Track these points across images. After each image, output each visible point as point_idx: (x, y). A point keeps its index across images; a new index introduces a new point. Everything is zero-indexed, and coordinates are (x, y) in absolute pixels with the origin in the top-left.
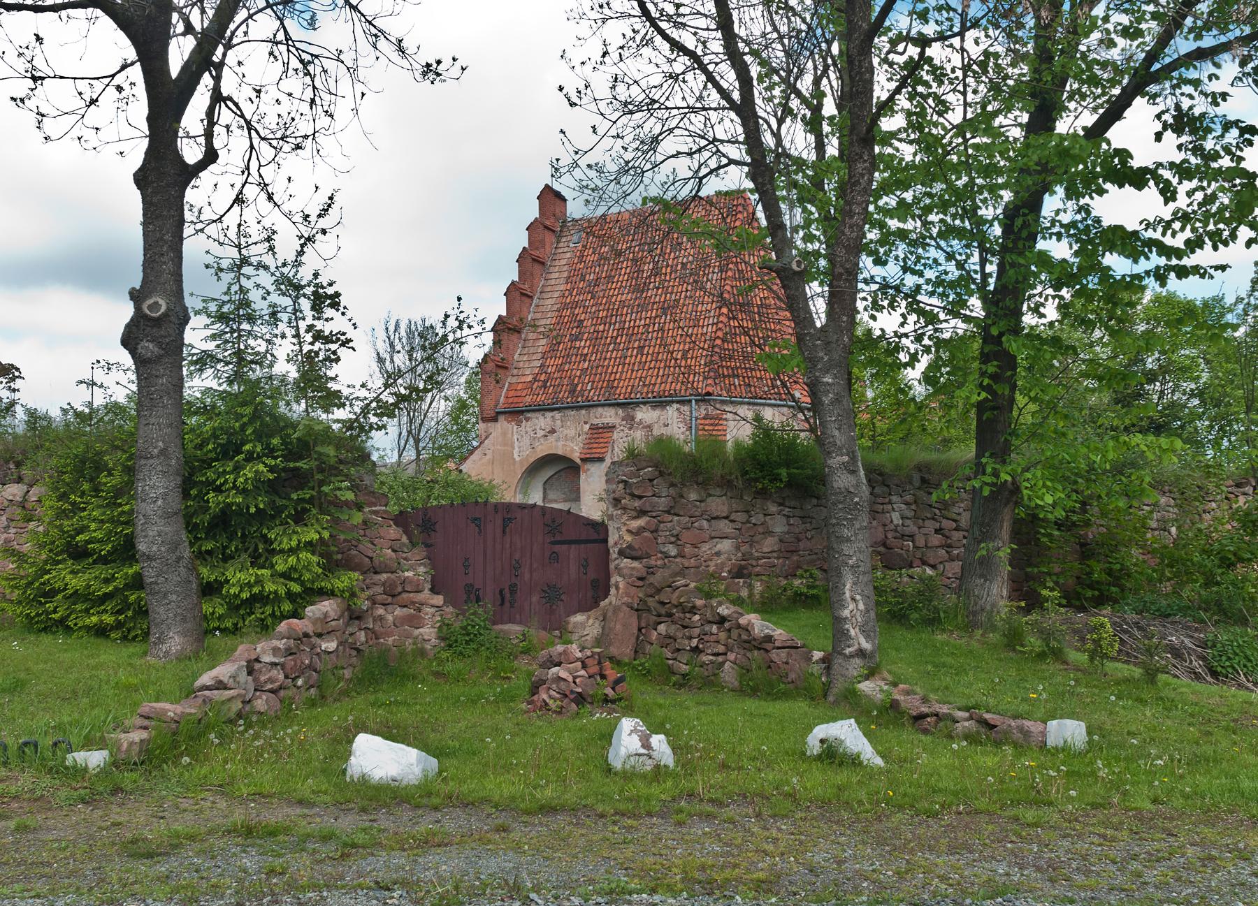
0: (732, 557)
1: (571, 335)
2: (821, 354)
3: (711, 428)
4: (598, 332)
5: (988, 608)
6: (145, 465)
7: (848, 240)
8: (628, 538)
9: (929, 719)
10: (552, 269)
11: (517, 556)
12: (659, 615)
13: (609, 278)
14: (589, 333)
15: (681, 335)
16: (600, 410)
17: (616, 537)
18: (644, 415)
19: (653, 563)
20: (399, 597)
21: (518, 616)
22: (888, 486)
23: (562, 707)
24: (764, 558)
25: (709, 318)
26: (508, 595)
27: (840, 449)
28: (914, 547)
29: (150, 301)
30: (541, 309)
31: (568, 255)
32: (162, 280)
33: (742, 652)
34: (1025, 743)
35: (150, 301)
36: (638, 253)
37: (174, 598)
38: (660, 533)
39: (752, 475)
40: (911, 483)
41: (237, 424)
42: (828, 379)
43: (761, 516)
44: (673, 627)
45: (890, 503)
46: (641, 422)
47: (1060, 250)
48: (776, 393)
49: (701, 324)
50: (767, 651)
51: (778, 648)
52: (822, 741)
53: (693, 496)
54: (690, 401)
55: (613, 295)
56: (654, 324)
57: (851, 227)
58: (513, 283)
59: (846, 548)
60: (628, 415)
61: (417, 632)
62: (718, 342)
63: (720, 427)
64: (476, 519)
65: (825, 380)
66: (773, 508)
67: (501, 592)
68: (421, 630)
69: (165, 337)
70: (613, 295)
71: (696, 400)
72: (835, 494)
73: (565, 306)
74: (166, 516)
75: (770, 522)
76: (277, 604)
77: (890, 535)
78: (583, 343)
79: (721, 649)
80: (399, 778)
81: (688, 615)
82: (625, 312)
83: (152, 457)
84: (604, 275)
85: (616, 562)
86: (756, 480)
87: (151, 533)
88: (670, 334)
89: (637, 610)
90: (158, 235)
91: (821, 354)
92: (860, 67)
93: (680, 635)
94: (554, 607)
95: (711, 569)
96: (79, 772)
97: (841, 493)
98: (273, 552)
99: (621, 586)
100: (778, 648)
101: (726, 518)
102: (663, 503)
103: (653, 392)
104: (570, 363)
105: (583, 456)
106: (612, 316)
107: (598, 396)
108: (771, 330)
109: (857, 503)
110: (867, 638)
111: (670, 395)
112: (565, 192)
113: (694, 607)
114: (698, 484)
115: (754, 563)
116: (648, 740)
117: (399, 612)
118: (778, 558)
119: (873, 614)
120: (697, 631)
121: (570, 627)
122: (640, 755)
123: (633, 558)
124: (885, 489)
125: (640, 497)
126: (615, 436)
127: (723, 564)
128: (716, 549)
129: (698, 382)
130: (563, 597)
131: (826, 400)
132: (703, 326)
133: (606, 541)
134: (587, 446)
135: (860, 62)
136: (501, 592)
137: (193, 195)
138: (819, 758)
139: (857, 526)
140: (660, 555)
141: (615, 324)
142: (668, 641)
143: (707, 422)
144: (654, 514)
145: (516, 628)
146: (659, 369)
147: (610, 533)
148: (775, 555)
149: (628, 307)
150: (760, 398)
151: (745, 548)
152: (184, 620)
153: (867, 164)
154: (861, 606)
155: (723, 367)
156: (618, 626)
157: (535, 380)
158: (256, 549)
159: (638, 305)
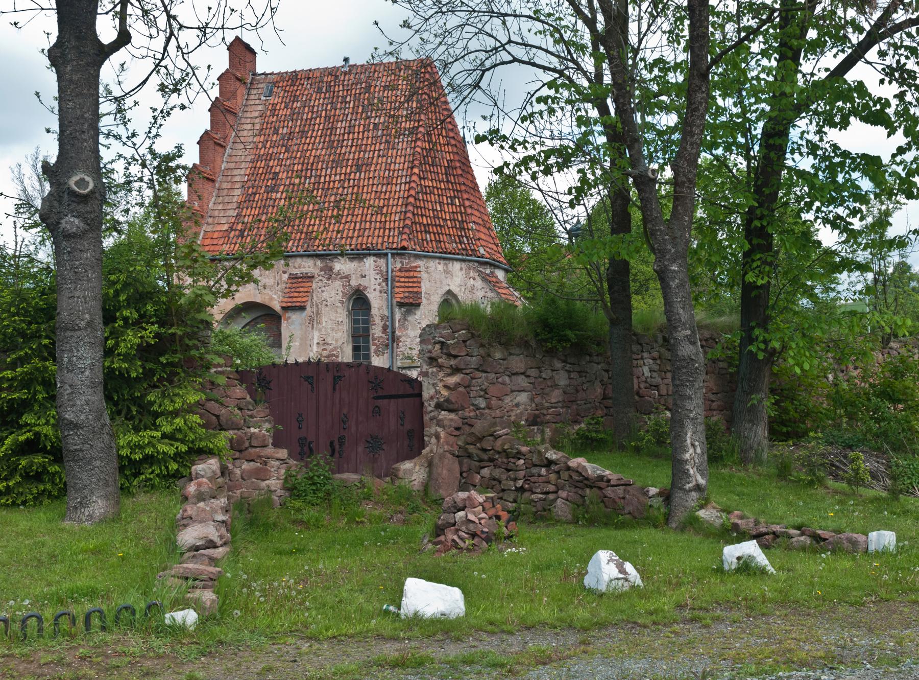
0: (528, 407)
1: (266, 186)
2: (669, 247)
3: (406, 280)
4: (294, 185)
5: (755, 446)
6: (72, 337)
7: (690, 155)
8: (445, 393)
9: (767, 537)
10: (243, 121)
11: (345, 411)
12: (481, 461)
13: (303, 133)
14: (285, 185)
15: (376, 192)
16: (299, 260)
17: (432, 392)
18: (341, 266)
19: (467, 414)
20: (246, 452)
21: (345, 466)
22: (641, 345)
23: (474, 545)
24: (552, 407)
25: (402, 176)
26: (337, 447)
27: (684, 324)
28: (659, 395)
29: (76, 178)
30: (234, 159)
31: (260, 108)
32: (83, 157)
33: (573, 490)
34: (854, 548)
35: (76, 178)
36: (331, 111)
37: (98, 463)
38: (472, 388)
39: (543, 336)
40: (656, 342)
41: (112, 291)
42: (674, 268)
43: (549, 371)
44: (498, 470)
45: (642, 358)
46: (339, 273)
47: (806, 164)
48: (463, 249)
49: (394, 182)
50: (600, 488)
51: (613, 486)
52: (739, 558)
53: (498, 355)
54: (386, 254)
55: (307, 150)
56: (349, 180)
57: (692, 144)
58: (206, 132)
59: (689, 405)
60: (327, 266)
61: (263, 484)
62: (411, 200)
63: (415, 280)
64: (309, 378)
65: (673, 268)
66: (558, 365)
67: (332, 443)
68: (267, 482)
69: (91, 213)
70: (307, 150)
71: (393, 254)
72: (680, 361)
73: (259, 158)
74: (93, 385)
75: (557, 377)
76: (163, 464)
77: (642, 386)
78: (279, 195)
79: (551, 488)
80: (447, 612)
81: (512, 460)
82: (319, 167)
83: (80, 329)
84: (297, 130)
85: (432, 414)
86: (546, 341)
87: (78, 403)
88: (365, 190)
89: (458, 457)
90: (79, 113)
91: (669, 247)
92: (700, 15)
93: (504, 477)
94: (377, 456)
95: (513, 418)
96: (178, 630)
97: (685, 360)
98: (156, 415)
99: (442, 435)
100: (613, 486)
101: (522, 374)
102: (474, 361)
103: (350, 245)
104: (267, 214)
105: (284, 305)
106: (307, 170)
107: (297, 246)
108: (457, 191)
109: (697, 368)
110: (702, 475)
111: (368, 249)
112: (255, 45)
113: (519, 452)
114: (501, 344)
115: (545, 412)
116: (622, 567)
117: (246, 466)
118: (562, 407)
119: (706, 457)
120: (522, 473)
121: (401, 474)
122: (618, 579)
123: (450, 411)
124: (639, 347)
125: (455, 357)
126: (314, 285)
127: (521, 413)
128: (516, 401)
129: (394, 236)
130: (384, 447)
131: (673, 284)
132: (396, 185)
133: (420, 395)
134: (287, 295)
135: (700, 11)
136: (332, 443)
137: (108, 72)
138: (738, 570)
139: (697, 386)
140: (472, 407)
141: (310, 178)
142: (494, 483)
143: (403, 274)
144: (468, 371)
145: (353, 477)
146: (355, 223)
147: (424, 388)
148: (560, 404)
149: (323, 161)
150: (450, 253)
151: (538, 400)
152: (107, 485)
153: (704, 95)
154: (699, 450)
155: (416, 224)
156: (444, 472)
157: (231, 229)
158: (129, 410)
159: (333, 161)
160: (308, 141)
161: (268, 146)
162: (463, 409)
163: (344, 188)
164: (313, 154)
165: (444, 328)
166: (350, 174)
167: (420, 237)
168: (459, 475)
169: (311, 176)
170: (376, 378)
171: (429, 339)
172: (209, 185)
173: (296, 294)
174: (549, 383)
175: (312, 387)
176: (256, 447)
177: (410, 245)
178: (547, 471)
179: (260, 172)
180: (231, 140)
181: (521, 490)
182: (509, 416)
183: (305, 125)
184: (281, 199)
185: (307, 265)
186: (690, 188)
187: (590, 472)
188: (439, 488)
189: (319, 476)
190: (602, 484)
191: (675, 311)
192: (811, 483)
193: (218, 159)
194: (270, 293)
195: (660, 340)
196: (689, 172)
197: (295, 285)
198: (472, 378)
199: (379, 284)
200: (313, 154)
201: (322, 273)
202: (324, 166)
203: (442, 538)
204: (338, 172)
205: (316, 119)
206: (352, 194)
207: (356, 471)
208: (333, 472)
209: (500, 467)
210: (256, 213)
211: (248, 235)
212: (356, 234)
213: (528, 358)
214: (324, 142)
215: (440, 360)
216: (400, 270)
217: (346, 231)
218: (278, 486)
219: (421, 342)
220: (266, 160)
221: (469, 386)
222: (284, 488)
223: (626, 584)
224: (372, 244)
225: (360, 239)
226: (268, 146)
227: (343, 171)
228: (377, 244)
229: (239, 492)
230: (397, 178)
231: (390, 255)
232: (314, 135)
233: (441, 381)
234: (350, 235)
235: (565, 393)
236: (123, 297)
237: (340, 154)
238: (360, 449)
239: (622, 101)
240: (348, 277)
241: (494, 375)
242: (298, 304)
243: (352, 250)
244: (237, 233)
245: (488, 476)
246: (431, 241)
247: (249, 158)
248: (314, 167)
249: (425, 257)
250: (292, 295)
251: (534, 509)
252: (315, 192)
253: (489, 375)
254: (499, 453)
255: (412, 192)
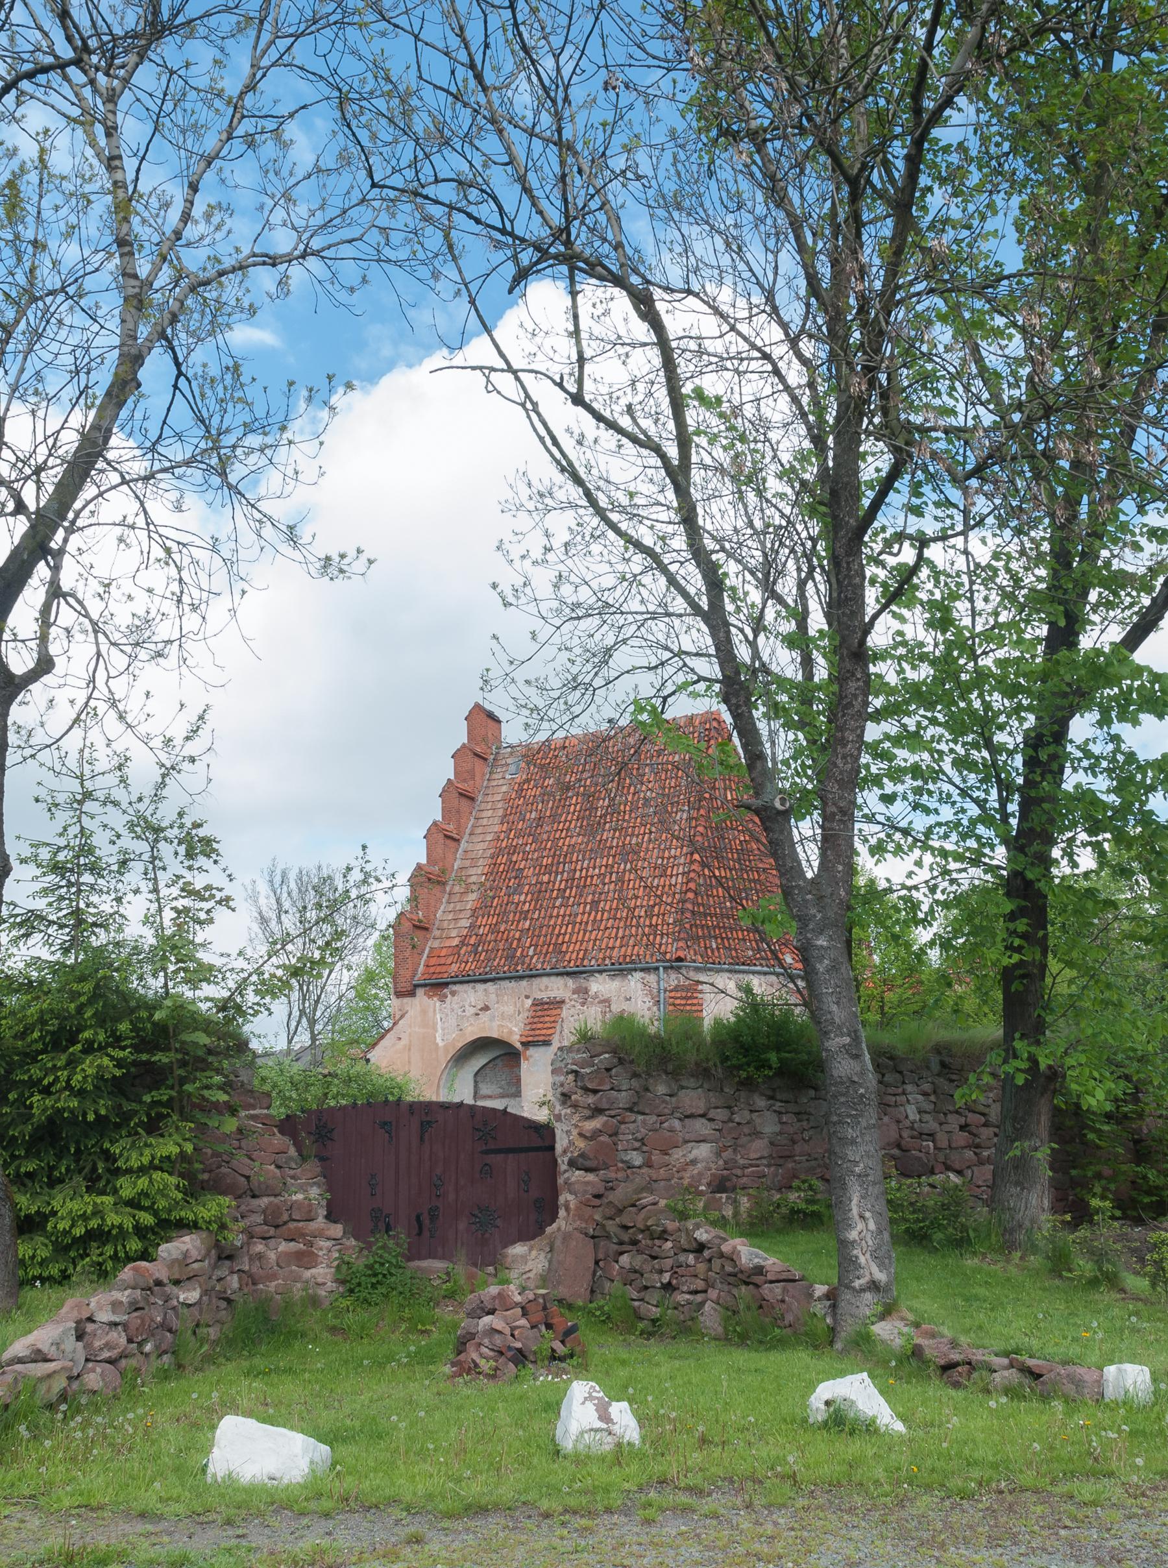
0: (713, 1166)
2: (813, 911)
5: (1027, 1224)
7: (841, 773)
12: (621, 1243)
13: (554, 817)
16: (545, 980)
17: (565, 1142)
18: (600, 985)
19: (612, 1175)
21: (440, 1249)
22: (900, 1072)
26: (426, 1221)
27: (839, 1027)
28: (935, 1148)
33: (726, 1288)
39: (735, 1062)
40: (928, 1068)
41: (73, 1006)
42: (822, 942)
43: (746, 1113)
44: (640, 1258)
45: (904, 1093)
46: (596, 996)
50: (757, 1286)
51: (771, 1282)
53: (661, 1089)
54: (657, 969)
57: (844, 757)
59: (851, 1153)
61: (308, 1274)
62: (690, 895)
64: (385, 1123)
65: (819, 943)
66: (761, 1103)
68: (313, 1271)
71: (665, 968)
72: (836, 1084)
75: (758, 1121)
77: (905, 1134)
78: (522, 898)
80: (278, 1475)
81: (657, 1242)
86: (739, 1067)
89: (593, 1237)
91: (813, 911)
93: (647, 1268)
97: (842, 1083)
101: (703, 1116)
102: (623, 1098)
109: (862, 1096)
110: (882, 1266)
111: (632, 962)
114: (667, 1073)
115: (739, 1172)
116: (606, 1410)
117: (284, 1246)
118: (769, 1166)
119: (886, 1236)
120: (668, 1263)
123: (587, 1170)
125: (595, 1092)
126: (564, 1013)
127: (700, 1174)
128: (691, 1156)
130: (499, 1222)
131: (821, 968)
133: (552, 1148)
139: (864, 1123)
144: (613, 1113)
148: (765, 1162)
153: (861, 683)
154: (872, 1226)
157: (463, 943)
165: (578, 1051)
170: (485, 1124)
172: (436, 890)
178: (696, 1259)
186: (844, 822)
192: (1094, 1283)
195: (935, 1067)
196: (840, 798)
208: (409, 1259)
212: (618, 943)
221: (616, 1134)
223: (609, 1439)
235: (772, 1143)
236: (88, 1014)
239: (734, 701)
240: (607, 1002)
241: (654, 1118)
245: (628, 1266)
249: (710, 970)
254: (642, 1231)
255: (692, 885)
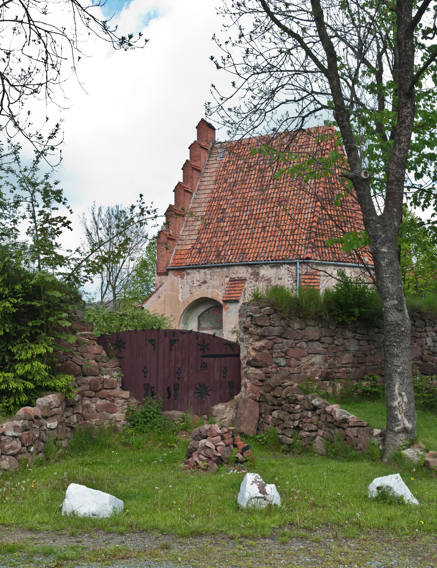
0: (322, 366)
1: (218, 218)
2: (380, 233)
7: (398, 159)
8: (253, 353)
10: (205, 175)
11: (179, 365)
12: (273, 405)
16: (236, 268)
18: (265, 272)
19: (269, 370)
20: (100, 393)
21: (179, 405)
22: (424, 320)
23: (208, 466)
24: (343, 367)
25: (309, 208)
26: (173, 391)
27: (392, 295)
30: (198, 201)
31: (216, 165)
33: (328, 429)
38: (275, 350)
39: (336, 313)
42: (384, 250)
43: (341, 340)
44: (283, 413)
45: (425, 331)
48: (352, 259)
49: (303, 212)
50: (344, 429)
51: (351, 427)
53: (296, 326)
54: (296, 263)
56: (273, 212)
57: (400, 150)
58: (179, 183)
59: (396, 362)
60: (255, 272)
61: (111, 416)
62: (315, 224)
63: (316, 281)
64: (152, 340)
66: (349, 334)
67: (168, 389)
68: (114, 414)
71: (300, 263)
72: (389, 325)
75: (347, 344)
77: (425, 353)
78: (225, 224)
79: (314, 427)
80: (97, 513)
81: (292, 405)
82: (253, 204)
84: (239, 179)
85: (245, 370)
86: (338, 316)
89: (259, 402)
91: (380, 233)
93: (287, 418)
94: (204, 399)
95: (308, 374)
97: (392, 325)
98: (15, 361)
99: (248, 385)
100: (351, 427)
101: (318, 340)
102: (276, 330)
103: (271, 257)
105: (225, 299)
106: (245, 206)
109: (403, 331)
110: (409, 420)
111: (283, 259)
113: (296, 400)
114: (300, 318)
115: (336, 370)
116: (264, 488)
117: (100, 402)
118: (352, 367)
119: (413, 405)
120: (298, 415)
121: (214, 413)
122: (258, 498)
123: (257, 367)
125: (261, 327)
126: (246, 286)
127: (315, 371)
128: (311, 361)
129: (301, 250)
130: (210, 393)
131: (383, 263)
132: (305, 214)
133: (238, 355)
134: (227, 292)
135: (405, 43)
136: (168, 389)
139: (403, 346)
140: (274, 365)
141: (246, 211)
143: (307, 277)
144: (271, 338)
146: (275, 241)
148: (350, 365)
149: (256, 200)
150: (342, 262)
151: (330, 361)
153: (410, 110)
154: (405, 399)
157: (193, 248)
159: (262, 199)
160: (246, 187)
161: (220, 191)
162: (267, 366)
163: (269, 218)
164: (249, 195)
165: (253, 305)
166: (273, 207)
167: (320, 251)
168: (258, 416)
169: (247, 210)
170: (204, 342)
171: (244, 314)
173: (233, 292)
174: (341, 349)
175: (155, 348)
176: (107, 389)
177: (313, 256)
178: (312, 414)
179: (214, 209)
180: (197, 188)
181: (297, 428)
182: (306, 373)
183: (245, 176)
184: (226, 227)
185: (242, 271)
187: (337, 415)
188: (241, 424)
189: (150, 412)
190: (345, 426)
191: (385, 284)
193: (187, 201)
194: (217, 291)
197: (233, 285)
198: (275, 343)
199: (291, 284)
200: (249, 195)
201: (252, 277)
202: (256, 203)
203: (190, 460)
204: (265, 207)
205: (252, 171)
206: (274, 221)
207: (181, 410)
209: (284, 410)
210: (210, 237)
211: (204, 252)
212: (275, 249)
213: (323, 329)
214: (257, 187)
215: (250, 329)
216: (306, 274)
217: (269, 247)
218: (122, 418)
219: (239, 316)
220: (218, 200)
222: (126, 420)
223: (265, 502)
224: (286, 256)
225: (278, 252)
226: (220, 191)
227: (269, 206)
228: (290, 256)
229: (94, 420)
230: (306, 209)
231: (298, 263)
232: (251, 182)
233: (251, 344)
234: (271, 250)
235: (354, 356)
237: (267, 194)
238: (191, 394)
239: (341, 119)
240: (269, 280)
241: (293, 341)
242: (234, 299)
243: (272, 260)
244: (197, 250)
245: (276, 417)
246: (329, 253)
247: (207, 200)
248: (249, 204)
249: (324, 264)
250: (230, 292)
251: (304, 444)
252: (249, 221)
253: (289, 341)
254: (285, 399)
